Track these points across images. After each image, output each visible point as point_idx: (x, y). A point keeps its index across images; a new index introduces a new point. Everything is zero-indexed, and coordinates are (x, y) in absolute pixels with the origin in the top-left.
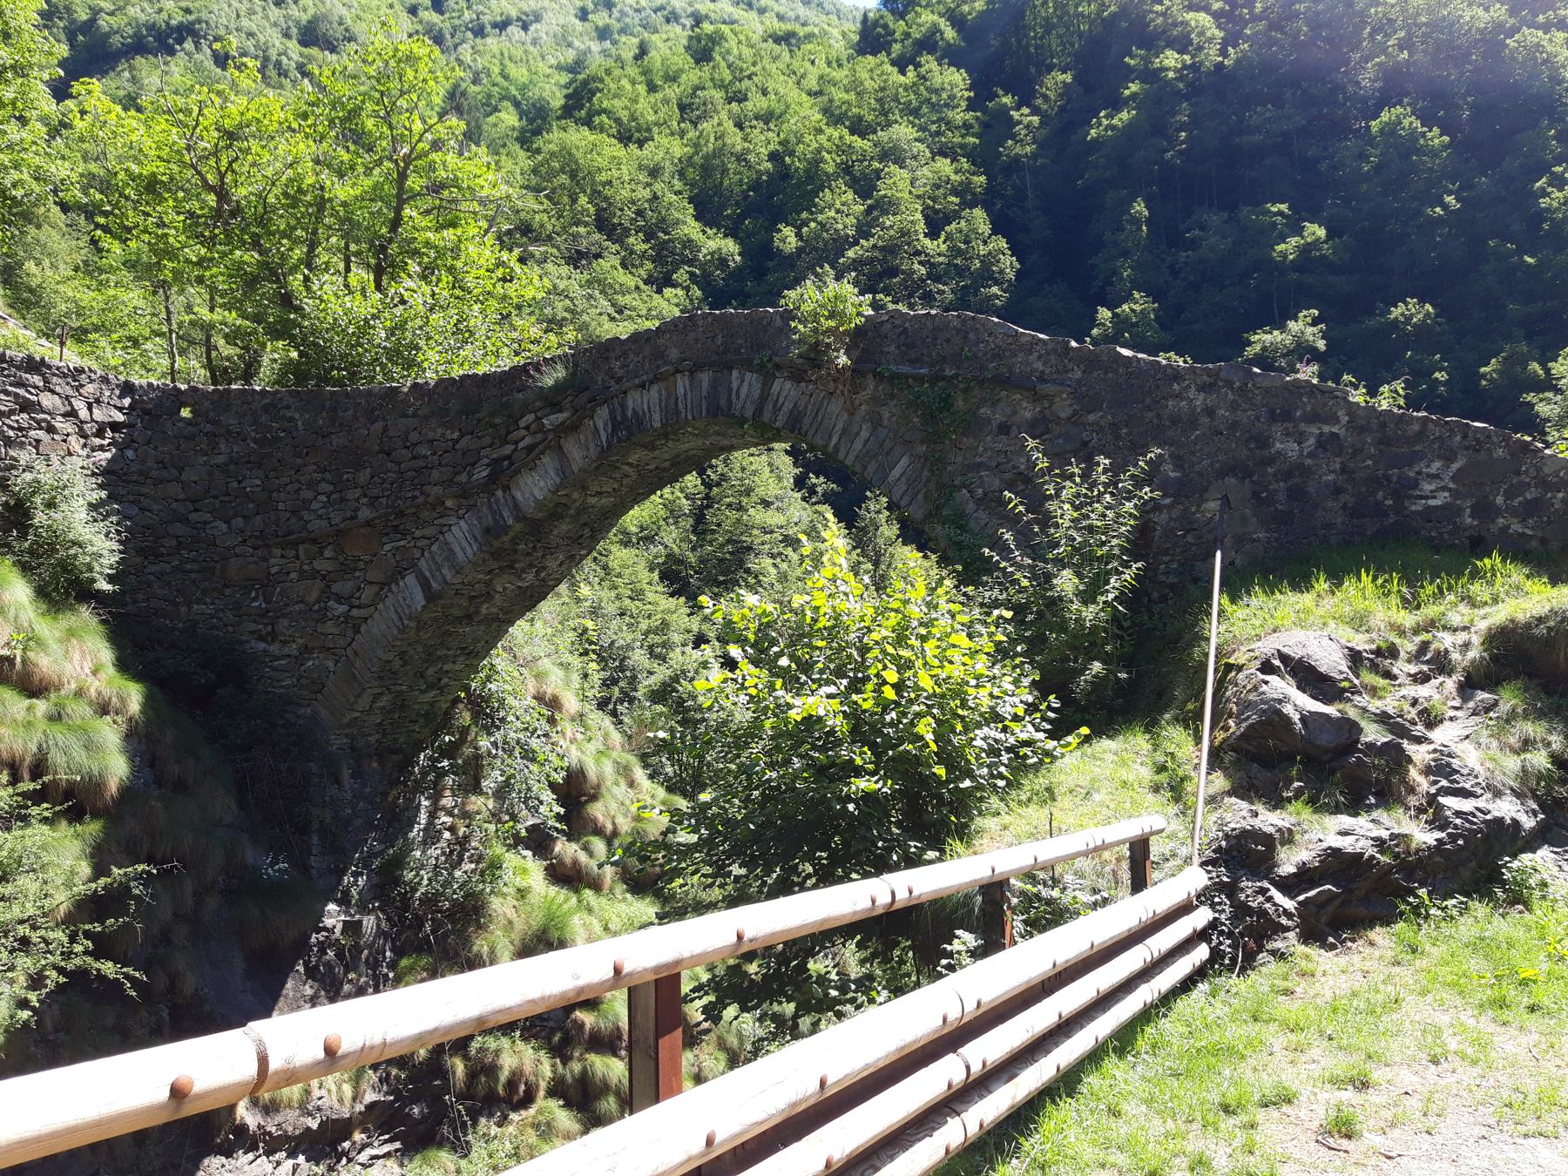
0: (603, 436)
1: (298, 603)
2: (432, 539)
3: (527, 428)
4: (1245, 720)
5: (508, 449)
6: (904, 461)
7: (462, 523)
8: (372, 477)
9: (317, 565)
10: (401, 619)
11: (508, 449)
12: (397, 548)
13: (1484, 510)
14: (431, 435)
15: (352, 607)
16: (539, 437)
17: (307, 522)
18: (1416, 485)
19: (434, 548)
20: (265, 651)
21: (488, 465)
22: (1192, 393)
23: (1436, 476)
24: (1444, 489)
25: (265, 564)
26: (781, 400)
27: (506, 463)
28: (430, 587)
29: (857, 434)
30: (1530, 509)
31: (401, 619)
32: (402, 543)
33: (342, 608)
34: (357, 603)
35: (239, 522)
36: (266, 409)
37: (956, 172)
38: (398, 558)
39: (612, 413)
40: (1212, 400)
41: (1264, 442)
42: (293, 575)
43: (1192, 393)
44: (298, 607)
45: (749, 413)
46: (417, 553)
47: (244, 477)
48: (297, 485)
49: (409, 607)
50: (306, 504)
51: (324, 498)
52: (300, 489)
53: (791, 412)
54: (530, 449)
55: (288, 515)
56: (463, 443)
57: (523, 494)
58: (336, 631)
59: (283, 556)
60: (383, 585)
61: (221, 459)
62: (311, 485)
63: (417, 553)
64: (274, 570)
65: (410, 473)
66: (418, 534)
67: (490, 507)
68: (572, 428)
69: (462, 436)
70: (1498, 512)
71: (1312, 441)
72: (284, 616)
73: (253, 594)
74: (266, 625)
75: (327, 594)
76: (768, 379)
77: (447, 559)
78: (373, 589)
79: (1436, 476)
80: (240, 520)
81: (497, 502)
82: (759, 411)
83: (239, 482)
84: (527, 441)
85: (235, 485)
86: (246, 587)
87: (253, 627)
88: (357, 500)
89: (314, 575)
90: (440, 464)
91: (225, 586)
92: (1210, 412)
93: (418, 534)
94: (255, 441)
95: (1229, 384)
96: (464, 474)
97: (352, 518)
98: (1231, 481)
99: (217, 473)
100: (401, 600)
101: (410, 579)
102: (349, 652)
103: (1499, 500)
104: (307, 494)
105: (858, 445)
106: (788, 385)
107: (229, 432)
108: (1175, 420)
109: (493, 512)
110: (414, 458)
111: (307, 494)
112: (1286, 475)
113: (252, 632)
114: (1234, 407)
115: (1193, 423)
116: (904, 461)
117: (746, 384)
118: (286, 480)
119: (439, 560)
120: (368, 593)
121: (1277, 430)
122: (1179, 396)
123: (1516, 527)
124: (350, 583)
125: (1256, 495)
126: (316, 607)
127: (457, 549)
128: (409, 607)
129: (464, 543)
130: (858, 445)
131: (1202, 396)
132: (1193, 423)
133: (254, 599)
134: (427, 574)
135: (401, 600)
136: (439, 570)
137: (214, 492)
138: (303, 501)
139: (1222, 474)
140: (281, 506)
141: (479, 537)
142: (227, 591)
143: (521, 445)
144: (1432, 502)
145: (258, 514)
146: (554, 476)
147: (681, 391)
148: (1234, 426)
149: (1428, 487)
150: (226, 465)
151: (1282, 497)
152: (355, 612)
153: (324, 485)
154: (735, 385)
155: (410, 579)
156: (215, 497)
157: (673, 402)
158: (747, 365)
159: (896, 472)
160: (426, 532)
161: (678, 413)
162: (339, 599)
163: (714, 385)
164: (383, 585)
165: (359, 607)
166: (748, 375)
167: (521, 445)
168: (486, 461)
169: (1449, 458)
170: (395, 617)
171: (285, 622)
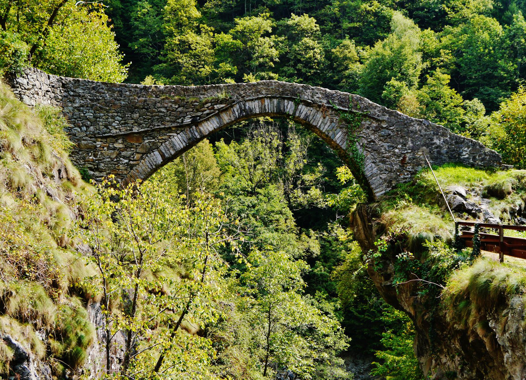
3: (207, 107)
5: (199, 114)
6: (340, 133)
7: (179, 135)
8: (139, 117)
9: (116, 145)
10: (152, 166)
11: (199, 114)
13: (474, 158)
14: (166, 105)
15: (130, 160)
16: (212, 111)
19: (167, 143)
21: (190, 118)
22: (416, 125)
25: (95, 144)
26: (302, 111)
28: (165, 156)
29: (326, 124)
31: (152, 166)
32: (153, 140)
33: (126, 161)
35: (84, 128)
36: (93, 88)
37: (346, 47)
42: (105, 148)
43: (416, 125)
44: (108, 160)
45: (291, 113)
47: (86, 112)
49: (155, 162)
50: (110, 124)
51: (117, 122)
53: (305, 115)
54: (208, 114)
58: (123, 168)
59: (101, 141)
60: (143, 154)
61: (77, 105)
62: (113, 117)
65: (156, 117)
66: (160, 138)
67: (190, 131)
68: (225, 110)
69: (179, 107)
70: (477, 160)
72: (102, 162)
73: (90, 154)
74: (94, 165)
75: (119, 155)
76: (297, 104)
77: (172, 147)
78: (140, 155)
80: (85, 128)
81: (193, 130)
82: (294, 113)
83: (84, 114)
84: (208, 111)
85: (83, 115)
87: (90, 166)
88: (132, 124)
91: (80, 151)
92: (420, 131)
93: (160, 138)
94: (90, 100)
95: (424, 124)
98: (424, 148)
104: (110, 120)
106: (304, 107)
108: (412, 132)
109: (192, 133)
110: (158, 112)
111: (110, 120)
112: (437, 147)
113: (89, 168)
114: (426, 130)
116: (340, 133)
117: (290, 104)
118: (102, 114)
119: (169, 147)
121: (435, 137)
122: (413, 126)
123: (480, 163)
124: (130, 152)
125: (430, 152)
126: (115, 160)
127: (176, 144)
128: (155, 162)
132: (416, 133)
133: (90, 156)
134: (164, 151)
136: (169, 150)
138: (109, 122)
139: (423, 146)
140: (100, 124)
142: (80, 153)
143: (205, 113)
145: (91, 126)
146: (217, 124)
147: (266, 104)
148: (425, 135)
149: (464, 153)
151: (435, 153)
152: (131, 162)
153: (118, 118)
154: (286, 104)
155: (156, 153)
156: (75, 119)
157: (263, 106)
158: (290, 99)
159: (338, 136)
160: (163, 137)
162: (124, 157)
163: (279, 103)
164: (143, 154)
165: (133, 161)
167: (205, 113)
168: (190, 116)
169: (468, 148)
170: (149, 165)
171: (103, 165)
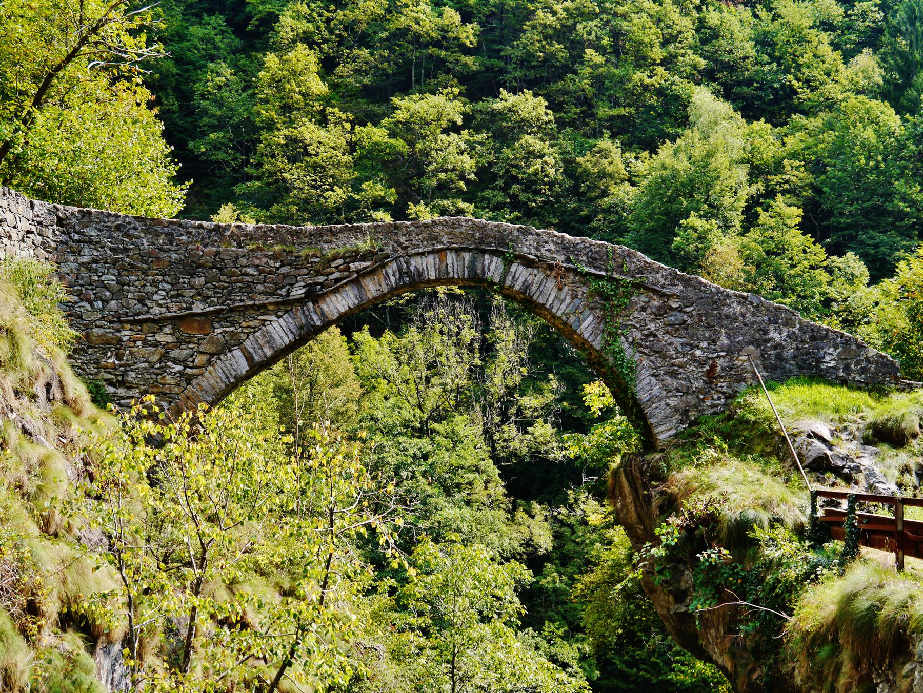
0: (393, 279)
1: (143, 362)
2: (255, 329)
3: (337, 267)
4: (250, 327)
5: (321, 279)
7: (281, 320)
8: (206, 283)
10: (228, 378)
11: (321, 279)
12: (227, 332)
13: (847, 368)
14: (257, 262)
16: (346, 273)
17: (149, 308)
18: (824, 358)
19: (258, 334)
20: (115, 393)
21: (304, 287)
22: (735, 305)
23: (831, 354)
24: (834, 360)
25: (119, 334)
26: (517, 276)
27: (319, 287)
29: (563, 301)
30: (864, 371)
31: (228, 378)
33: (179, 368)
34: (191, 365)
38: (227, 338)
39: (400, 268)
40: (744, 310)
41: (766, 332)
42: (139, 343)
43: (735, 305)
44: (143, 365)
46: (243, 337)
47: (103, 273)
48: (143, 283)
50: (149, 296)
51: (163, 293)
52: (145, 285)
54: (337, 280)
55: (135, 302)
56: (284, 270)
57: (329, 307)
58: (173, 382)
59: (131, 330)
60: (212, 355)
61: (85, 259)
62: (154, 284)
63: (243, 337)
64: (125, 339)
65: (239, 284)
66: (244, 324)
67: (303, 312)
68: (370, 273)
71: (785, 334)
72: (132, 370)
73: (109, 354)
74: (116, 375)
75: (165, 357)
76: (508, 263)
77: (268, 342)
78: (205, 358)
79: (831, 354)
81: (308, 309)
82: (503, 280)
83: (99, 276)
84: (337, 275)
85: (96, 278)
86: (104, 349)
88: (192, 297)
89: (157, 344)
90: (264, 282)
91: (89, 347)
92: (743, 315)
93: (244, 324)
94: (111, 249)
95: (751, 303)
96: (284, 290)
97: (187, 309)
98: (751, 347)
99: (82, 269)
100: (229, 366)
101: (237, 353)
102: (182, 396)
103: (853, 366)
104: (149, 289)
105: (564, 306)
106: (521, 268)
107: (91, 242)
108: (727, 317)
110: (242, 275)
111: (149, 289)
112: (775, 347)
113: (106, 380)
114: (753, 314)
115: (735, 319)
116: (590, 318)
118: (133, 278)
120: (200, 359)
121: (771, 328)
122: (729, 305)
125: (762, 356)
126: (158, 366)
129: (282, 334)
130: (564, 306)
131: (739, 307)
132: (735, 319)
133: (110, 358)
134: (251, 350)
135: (229, 366)
137: (81, 282)
139: (748, 344)
141: (294, 331)
142: (90, 351)
144: (830, 365)
145: (112, 299)
147: (449, 261)
148: (753, 323)
149: (828, 358)
150: (88, 263)
152: (189, 371)
153: (164, 284)
154: (487, 263)
155: (237, 353)
156: (82, 286)
159: (586, 324)
160: (251, 324)
161: (447, 273)
162: (176, 361)
163: (473, 261)
164: (212, 355)
165: (191, 368)
166: (495, 259)
167: (331, 277)
170: (223, 376)
171: (133, 374)
